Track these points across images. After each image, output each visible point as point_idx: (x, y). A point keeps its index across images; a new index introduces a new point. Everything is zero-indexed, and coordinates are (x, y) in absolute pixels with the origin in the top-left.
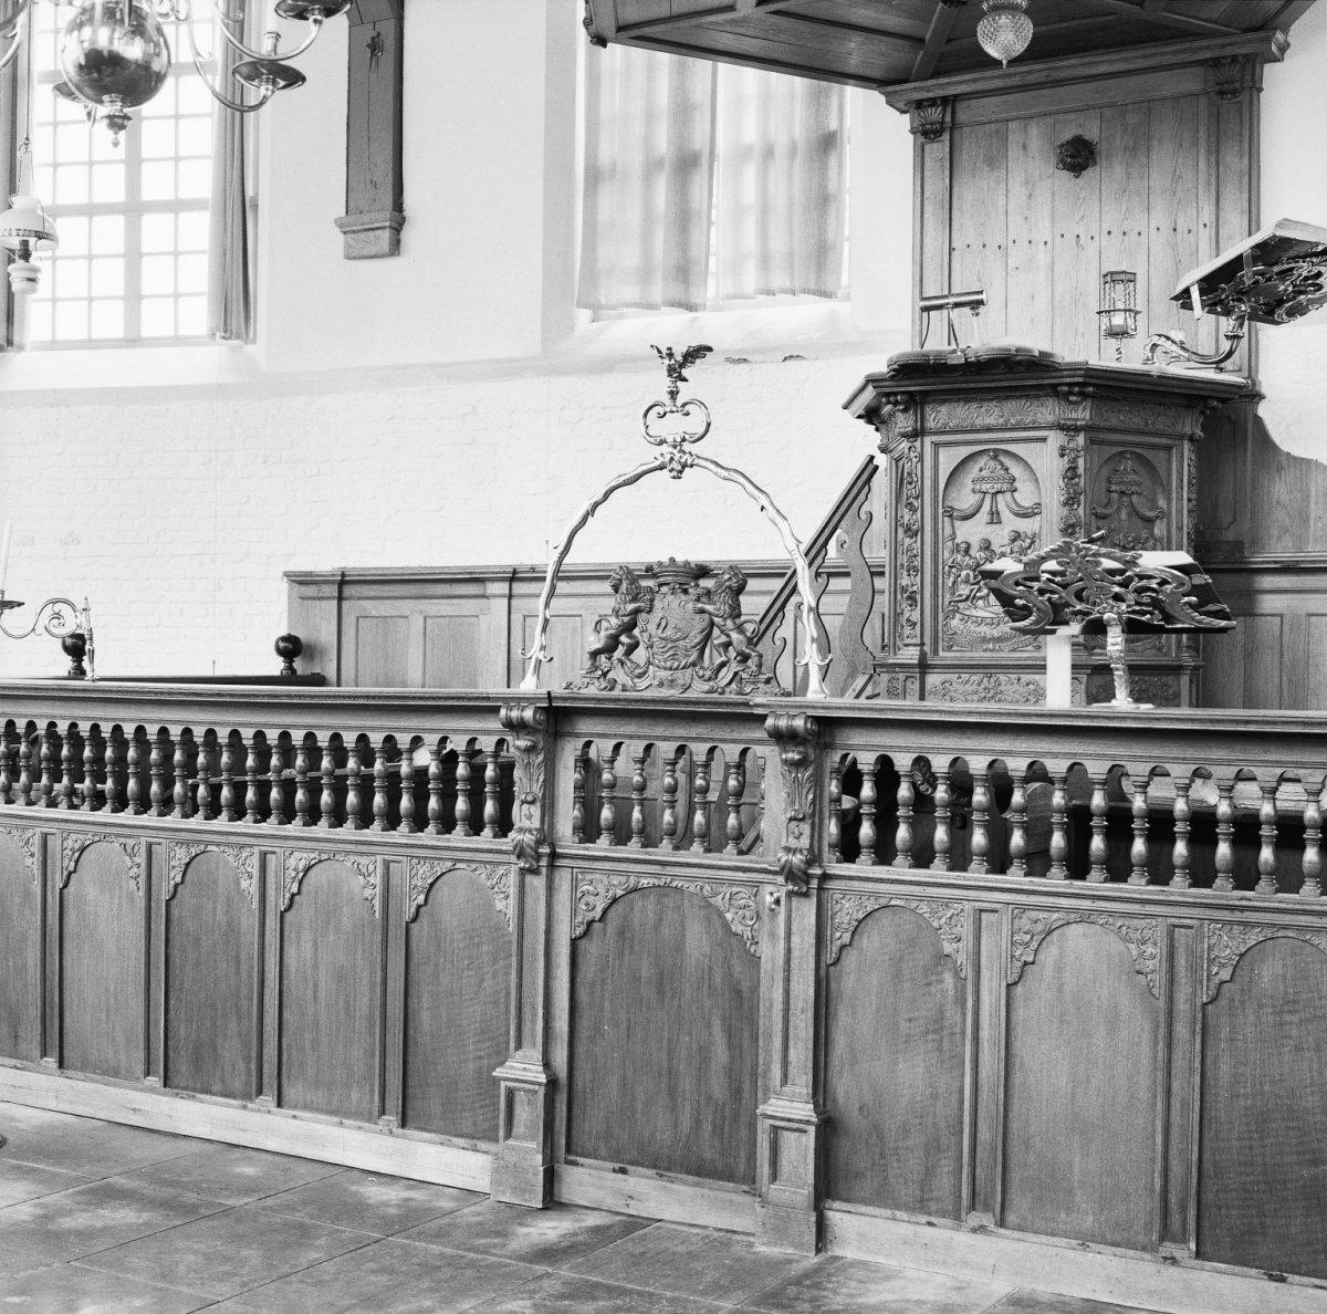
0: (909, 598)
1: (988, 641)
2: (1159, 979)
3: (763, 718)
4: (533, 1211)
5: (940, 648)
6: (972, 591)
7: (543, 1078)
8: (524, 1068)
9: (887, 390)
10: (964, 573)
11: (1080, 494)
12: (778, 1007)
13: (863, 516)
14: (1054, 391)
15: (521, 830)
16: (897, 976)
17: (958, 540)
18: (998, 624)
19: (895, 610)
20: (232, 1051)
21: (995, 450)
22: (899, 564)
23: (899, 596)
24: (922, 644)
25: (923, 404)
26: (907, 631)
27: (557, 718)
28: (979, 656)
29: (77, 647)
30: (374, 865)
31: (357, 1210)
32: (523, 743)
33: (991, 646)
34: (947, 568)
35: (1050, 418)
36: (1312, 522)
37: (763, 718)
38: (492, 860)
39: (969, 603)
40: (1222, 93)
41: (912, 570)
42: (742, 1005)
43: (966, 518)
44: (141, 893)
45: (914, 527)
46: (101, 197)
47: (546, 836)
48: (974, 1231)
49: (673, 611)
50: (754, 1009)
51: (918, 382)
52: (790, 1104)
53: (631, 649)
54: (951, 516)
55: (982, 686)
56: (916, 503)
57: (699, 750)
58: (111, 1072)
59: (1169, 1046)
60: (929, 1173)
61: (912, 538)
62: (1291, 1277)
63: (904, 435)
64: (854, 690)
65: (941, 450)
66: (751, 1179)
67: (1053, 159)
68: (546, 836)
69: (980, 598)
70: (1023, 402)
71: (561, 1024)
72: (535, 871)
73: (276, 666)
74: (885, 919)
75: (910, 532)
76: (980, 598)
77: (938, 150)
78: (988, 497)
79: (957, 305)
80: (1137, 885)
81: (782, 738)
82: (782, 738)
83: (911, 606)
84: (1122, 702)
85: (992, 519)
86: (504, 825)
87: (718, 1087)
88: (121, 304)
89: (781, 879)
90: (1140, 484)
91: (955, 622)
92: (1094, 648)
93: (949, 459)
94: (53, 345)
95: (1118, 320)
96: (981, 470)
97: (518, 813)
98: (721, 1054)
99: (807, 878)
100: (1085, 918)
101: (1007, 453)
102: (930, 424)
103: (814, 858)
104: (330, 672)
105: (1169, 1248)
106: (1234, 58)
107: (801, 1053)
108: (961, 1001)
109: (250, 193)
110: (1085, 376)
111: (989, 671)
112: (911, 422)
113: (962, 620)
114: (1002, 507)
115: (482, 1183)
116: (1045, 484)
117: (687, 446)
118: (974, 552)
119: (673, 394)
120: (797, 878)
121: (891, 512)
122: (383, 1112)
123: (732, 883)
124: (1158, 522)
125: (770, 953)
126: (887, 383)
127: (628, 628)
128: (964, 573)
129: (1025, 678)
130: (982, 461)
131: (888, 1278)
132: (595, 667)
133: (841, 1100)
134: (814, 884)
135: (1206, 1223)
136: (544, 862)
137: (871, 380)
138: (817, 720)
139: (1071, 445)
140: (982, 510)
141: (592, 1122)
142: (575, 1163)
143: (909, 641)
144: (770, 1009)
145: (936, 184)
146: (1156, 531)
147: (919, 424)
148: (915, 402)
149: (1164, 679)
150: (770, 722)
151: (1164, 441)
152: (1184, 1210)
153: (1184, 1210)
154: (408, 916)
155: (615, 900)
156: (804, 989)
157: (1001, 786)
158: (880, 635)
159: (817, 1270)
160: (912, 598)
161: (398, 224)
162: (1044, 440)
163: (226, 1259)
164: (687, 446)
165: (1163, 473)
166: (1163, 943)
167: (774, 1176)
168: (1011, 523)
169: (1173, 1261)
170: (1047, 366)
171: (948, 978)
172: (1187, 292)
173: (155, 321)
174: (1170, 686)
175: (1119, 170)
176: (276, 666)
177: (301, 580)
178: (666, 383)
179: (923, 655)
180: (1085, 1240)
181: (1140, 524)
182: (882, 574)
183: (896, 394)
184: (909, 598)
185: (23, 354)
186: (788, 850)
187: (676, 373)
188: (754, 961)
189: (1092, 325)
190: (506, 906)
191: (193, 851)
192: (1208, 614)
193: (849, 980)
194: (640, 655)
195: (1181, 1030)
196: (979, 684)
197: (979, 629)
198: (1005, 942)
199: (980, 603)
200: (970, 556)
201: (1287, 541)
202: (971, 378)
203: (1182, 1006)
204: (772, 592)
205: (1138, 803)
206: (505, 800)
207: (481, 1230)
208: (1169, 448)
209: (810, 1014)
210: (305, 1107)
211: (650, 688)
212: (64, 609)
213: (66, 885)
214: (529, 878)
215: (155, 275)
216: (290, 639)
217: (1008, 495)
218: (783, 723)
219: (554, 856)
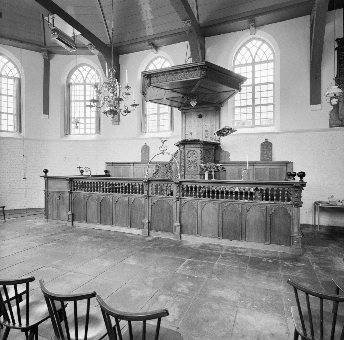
2: (218, 209)
3: (174, 181)
4: (147, 237)
7: (148, 222)
8: (146, 220)
12: (175, 213)
14: (200, 143)
15: (145, 194)
16: (189, 209)
20: (109, 219)
26: (183, 170)
27: (149, 181)
28: (190, 173)
30: (127, 198)
31: (127, 237)
32: (145, 184)
37: (174, 181)
38: (141, 197)
40: (216, 110)
42: (171, 213)
44: (97, 201)
46: (89, 119)
47: (148, 194)
48: (198, 237)
49: (163, 169)
50: (172, 213)
52: (177, 223)
53: (158, 173)
57: (162, 185)
58: (93, 223)
59: (219, 216)
60: (192, 230)
62: (233, 240)
66: (172, 232)
67: (197, 117)
68: (148, 194)
71: (150, 215)
72: (147, 198)
73: (104, 174)
74: (188, 203)
77: (184, 115)
79: (189, 134)
80: (215, 199)
81: (176, 183)
82: (176, 183)
84: (214, 179)
86: (142, 193)
87: (168, 222)
88: (83, 130)
89: (176, 199)
93: (187, 151)
94: (75, 134)
95: (206, 136)
97: (144, 191)
98: (169, 218)
99: (179, 199)
100: (210, 202)
102: (185, 147)
103: (179, 196)
104: (111, 174)
105: (219, 238)
106: (218, 106)
107: (178, 218)
108: (196, 212)
109: (100, 116)
115: (141, 234)
116: (198, 154)
117: (164, 151)
119: (163, 145)
120: (178, 199)
122: (128, 226)
123: (170, 199)
125: (174, 207)
127: (157, 171)
130: (191, 151)
131: (188, 242)
132: (153, 175)
133: (182, 222)
134: (179, 199)
135: (223, 235)
136: (148, 197)
137: (179, 142)
138: (180, 181)
141: (153, 226)
142: (152, 231)
144: (174, 213)
145: (184, 119)
148: (184, 145)
150: (175, 182)
152: (221, 233)
153: (221, 233)
154: (131, 204)
155: (156, 201)
156: (178, 211)
157: (192, 188)
159: (180, 242)
160: (183, 166)
161: (119, 121)
162: (198, 149)
163: (114, 244)
164: (164, 151)
166: (218, 205)
167: (175, 232)
168: (194, 158)
169: (220, 239)
171: (194, 209)
172: (215, 133)
173: (88, 131)
175: (205, 118)
177: (107, 163)
180: (210, 237)
185: (71, 135)
186: (177, 196)
187: (163, 142)
188: (172, 208)
189: (204, 136)
190: (143, 202)
191: (104, 196)
192: (224, 170)
193: (183, 209)
194: (159, 174)
195: (220, 214)
198: (201, 206)
201: (223, 160)
203: (220, 212)
205: (225, 191)
206: (143, 190)
207: (142, 239)
208: (211, 150)
209: (179, 213)
210: (118, 226)
211: (160, 178)
212: (87, 168)
213: (87, 201)
214: (146, 199)
215: (88, 126)
216: (106, 170)
218: (176, 182)
219: (149, 197)
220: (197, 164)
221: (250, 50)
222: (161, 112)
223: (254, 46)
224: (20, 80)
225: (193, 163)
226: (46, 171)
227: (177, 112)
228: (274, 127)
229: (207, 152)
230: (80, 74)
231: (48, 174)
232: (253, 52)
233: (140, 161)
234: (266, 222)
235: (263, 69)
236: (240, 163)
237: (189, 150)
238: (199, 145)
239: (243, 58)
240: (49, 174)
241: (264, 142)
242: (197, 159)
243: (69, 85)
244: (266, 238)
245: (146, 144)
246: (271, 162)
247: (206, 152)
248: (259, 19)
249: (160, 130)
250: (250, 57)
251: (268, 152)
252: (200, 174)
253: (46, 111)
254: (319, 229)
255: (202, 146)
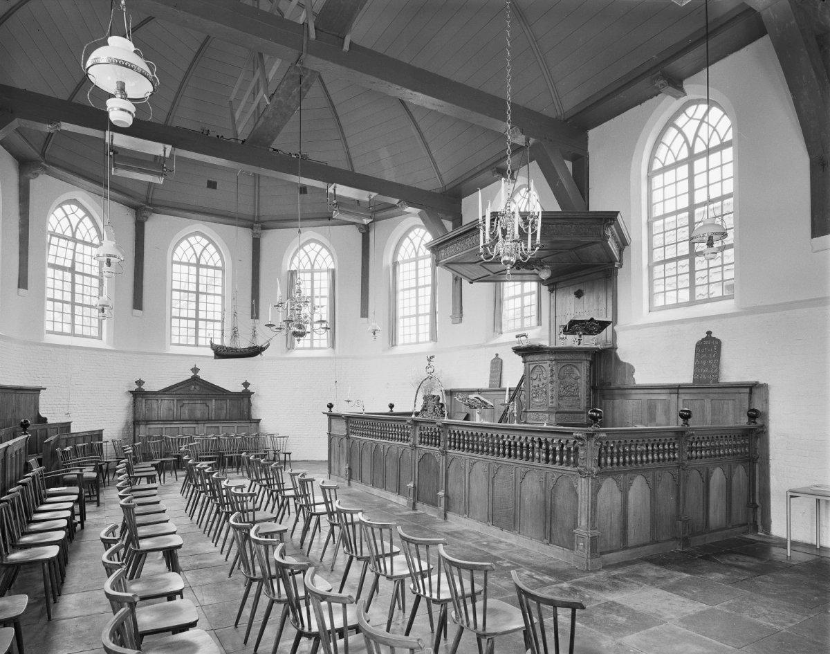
29: (391, 406)
66: (437, 506)
71: (417, 477)
73: (388, 410)
77: (553, 295)
176: (388, 410)
178: (428, 362)
221: (683, 129)
222: (420, 312)
223: (691, 118)
224: (333, 272)
226: (330, 406)
227: (545, 289)
228: (731, 302)
230: (680, 135)
231: (332, 409)
232: (312, 257)
233: (486, 386)
234: (545, 501)
235: (681, 179)
237: (564, 364)
239: (670, 152)
240: (334, 410)
241: (703, 340)
243: (395, 264)
244: (545, 533)
245: (709, 333)
246: (717, 385)
248: (680, 64)
249: (697, 299)
250: (683, 145)
251: (711, 362)
253: (364, 313)
254: (791, 550)
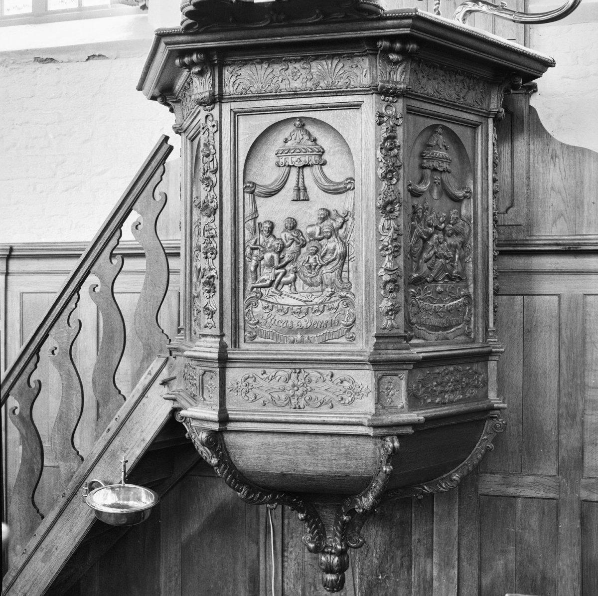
0: (206, 283)
1: (295, 332)
5: (242, 339)
6: (276, 276)
9: (181, 47)
10: (267, 256)
11: (399, 167)
13: (158, 197)
17: (260, 219)
18: (307, 313)
19: (191, 292)
21: (301, 119)
22: (194, 245)
23: (195, 279)
24: (222, 336)
25: (222, 66)
26: (205, 319)
28: (286, 349)
33: (299, 337)
34: (248, 250)
35: (367, 81)
36: (586, 207)
39: (273, 288)
41: (208, 253)
43: (271, 194)
45: (213, 205)
51: (218, 36)
54: (252, 193)
55: (290, 383)
56: (213, 178)
61: (209, 216)
63: (201, 103)
64: (149, 373)
65: (242, 119)
69: (287, 283)
70: (335, 62)
75: (208, 209)
76: (287, 283)
78: (294, 171)
83: (209, 292)
85: (298, 195)
90: (450, 162)
91: (258, 310)
92: (411, 338)
93: (250, 128)
96: (286, 141)
101: (315, 121)
102: (229, 89)
110: (412, 27)
111: (298, 366)
112: (208, 87)
113: (265, 308)
114: (309, 182)
118: (277, 232)
121: (186, 193)
124: (465, 202)
126: (181, 38)
128: (267, 256)
129: (339, 374)
130: (287, 131)
139: (389, 112)
140: (287, 186)
143: (207, 331)
146: (463, 212)
147: (217, 89)
149: (475, 367)
151: (472, 118)
158: (177, 312)
160: (209, 283)
165: (469, 151)
168: (320, 200)
170: (371, 12)
174: (480, 374)
179: (223, 348)
181: (450, 203)
182: (178, 255)
183: (189, 52)
184: (206, 283)
196: (286, 381)
197: (284, 318)
199: (286, 289)
200: (274, 237)
202: (280, 31)
204: (68, 272)
208: (474, 126)
217: (316, 169)
220: (344, 256)
225: (311, 246)
229: (442, 139)
236: (186, 276)
238: (365, 63)
242: (349, 206)
247: (427, 146)
252: (375, 363)
255: (399, 77)
